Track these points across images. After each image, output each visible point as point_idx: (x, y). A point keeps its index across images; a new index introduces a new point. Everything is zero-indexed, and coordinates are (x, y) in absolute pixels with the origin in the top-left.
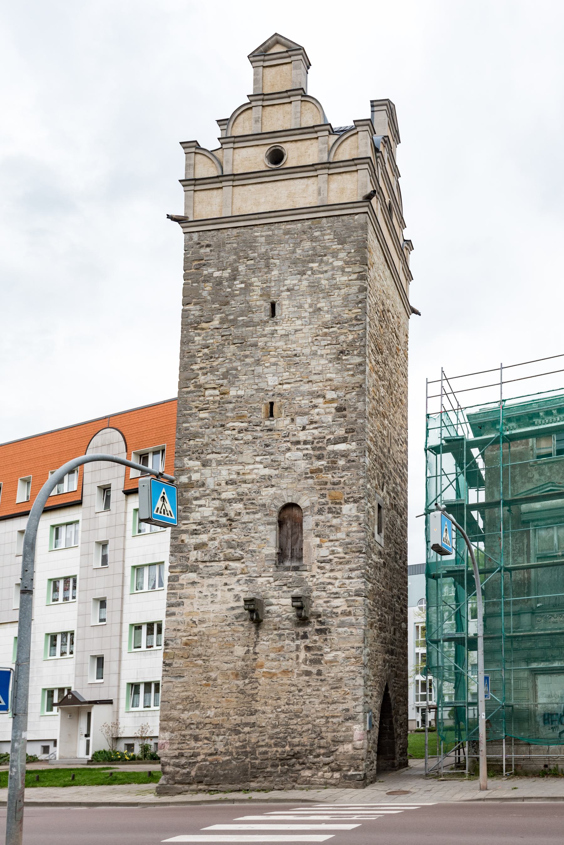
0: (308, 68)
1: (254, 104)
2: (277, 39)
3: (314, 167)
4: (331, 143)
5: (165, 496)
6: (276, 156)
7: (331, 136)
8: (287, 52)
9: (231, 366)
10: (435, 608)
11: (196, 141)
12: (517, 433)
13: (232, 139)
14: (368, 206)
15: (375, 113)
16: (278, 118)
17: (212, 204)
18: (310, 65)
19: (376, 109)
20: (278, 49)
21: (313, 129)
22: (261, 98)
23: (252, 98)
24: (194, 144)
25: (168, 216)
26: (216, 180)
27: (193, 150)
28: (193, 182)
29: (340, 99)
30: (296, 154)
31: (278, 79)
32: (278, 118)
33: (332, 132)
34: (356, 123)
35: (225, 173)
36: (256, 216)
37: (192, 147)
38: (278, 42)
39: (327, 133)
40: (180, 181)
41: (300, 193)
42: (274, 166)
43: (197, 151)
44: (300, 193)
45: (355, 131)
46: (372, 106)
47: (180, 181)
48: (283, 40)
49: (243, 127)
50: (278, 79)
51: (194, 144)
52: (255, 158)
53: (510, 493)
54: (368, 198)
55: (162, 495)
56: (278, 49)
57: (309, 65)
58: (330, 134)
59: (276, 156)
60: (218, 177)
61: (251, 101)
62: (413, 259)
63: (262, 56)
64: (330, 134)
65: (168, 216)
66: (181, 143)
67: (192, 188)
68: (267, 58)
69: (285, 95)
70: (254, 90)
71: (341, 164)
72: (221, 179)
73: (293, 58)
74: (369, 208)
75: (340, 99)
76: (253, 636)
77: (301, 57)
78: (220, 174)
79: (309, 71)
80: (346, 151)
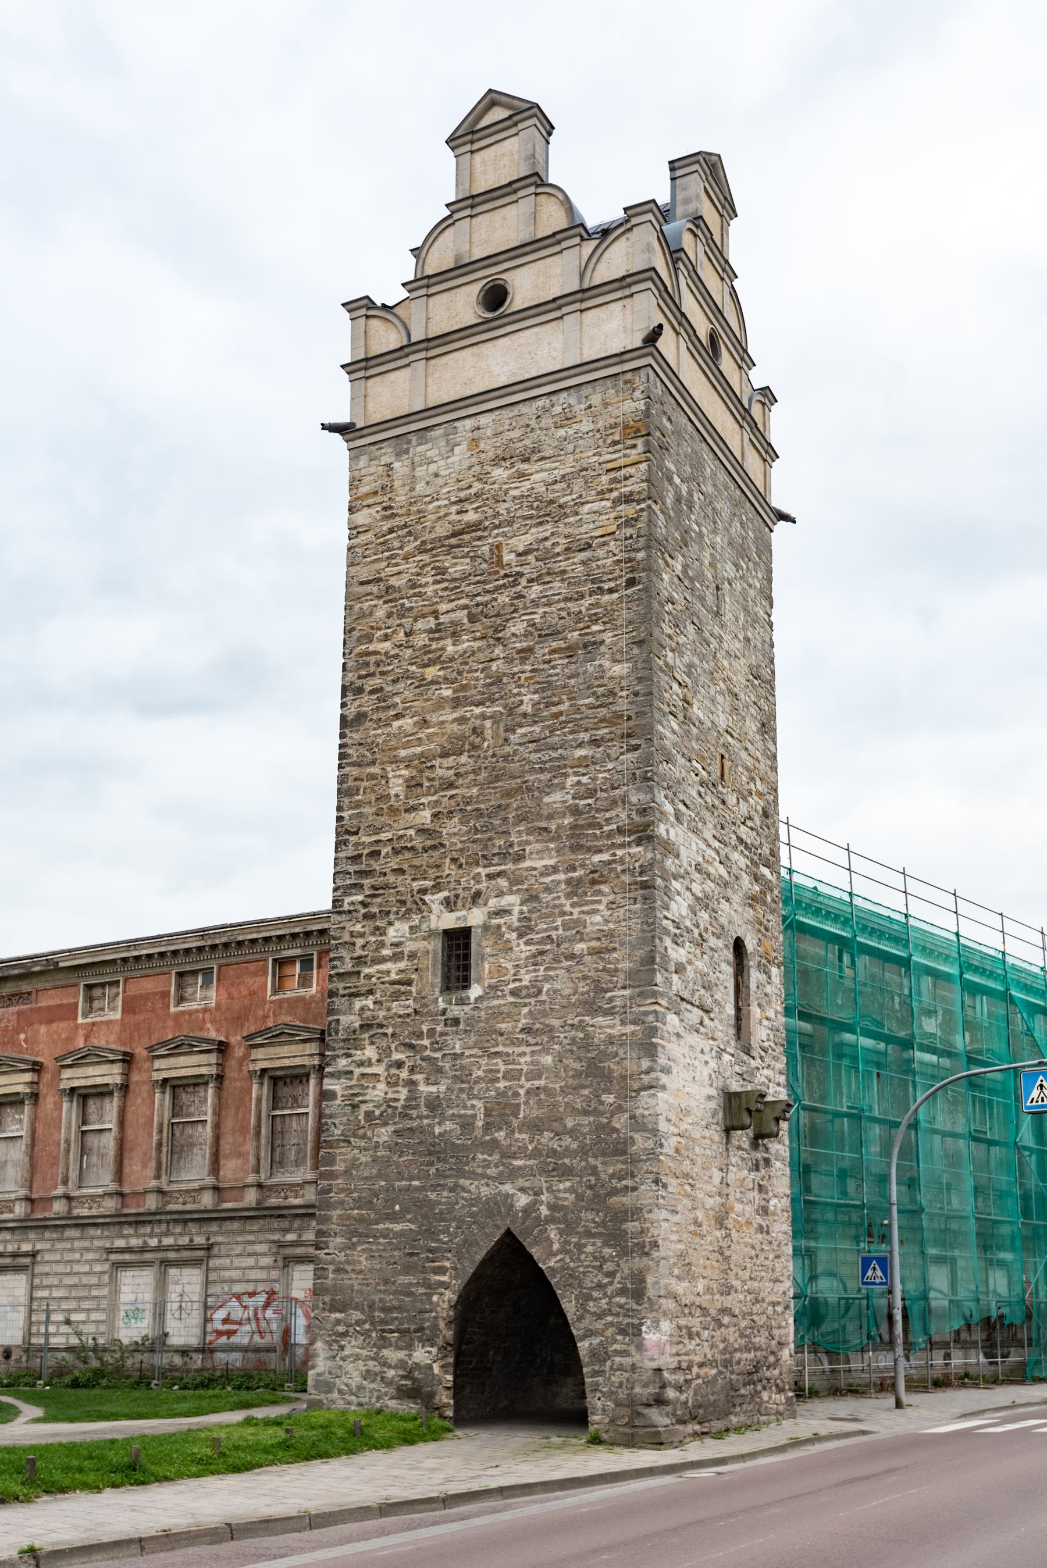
0: (550, 134)
1: (456, 216)
2: (492, 99)
3: (556, 303)
4: (585, 258)
6: (495, 297)
8: (510, 117)
11: (367, 297)
13: (425, 281)
14: (651, 354)
15: (678, 181)
16: (501, 228)
18: (553, 128)
19: (678, 173)
20: (498, 114)
21: (555, 238)
22: (469, 204)
23: (453, 208)
24: (365, 301)
25: (324, 427)
27: (363, 311)
29: (604, 173)
30: (526, 286)
31: (500, 163)
32: (501, 228)
33: (586, 236)
34: (629, 212)
35: (413, 340)
36: (463, 404)
37: (362, 308)
38: (493, 104)
39: (577, 240)
41: (540, 349)
42: (490, 315)
43: (371, 313)
44: (540, 349)
45: (629, 226)
46: (672, 169)
48: (504, 99)
49: (439, 259)
50: (500, 163)
51: (365, 301)
52: (461, 306)
54: (654, 336)
56: (498, 114)
57: (550, 128)
58: (583, 239)
59: (495, 297)
60: (402, 348)
61: (453, 212)
62: (779, 426)
63: (466, 138)
64: (583, 239)
65: (324, 427)
66: (404, 285)
67: (361, 374)
68: (476, 136)
69: (508, 189)
70: (457, 193)
71: (388, 357)
72: (407, 350)
73: (521, 126)
75: (604, 173)
76: (722, 1149)
77: (534, 121)
78: (405, 343)
79: (551, 139)
80: (617, 261)
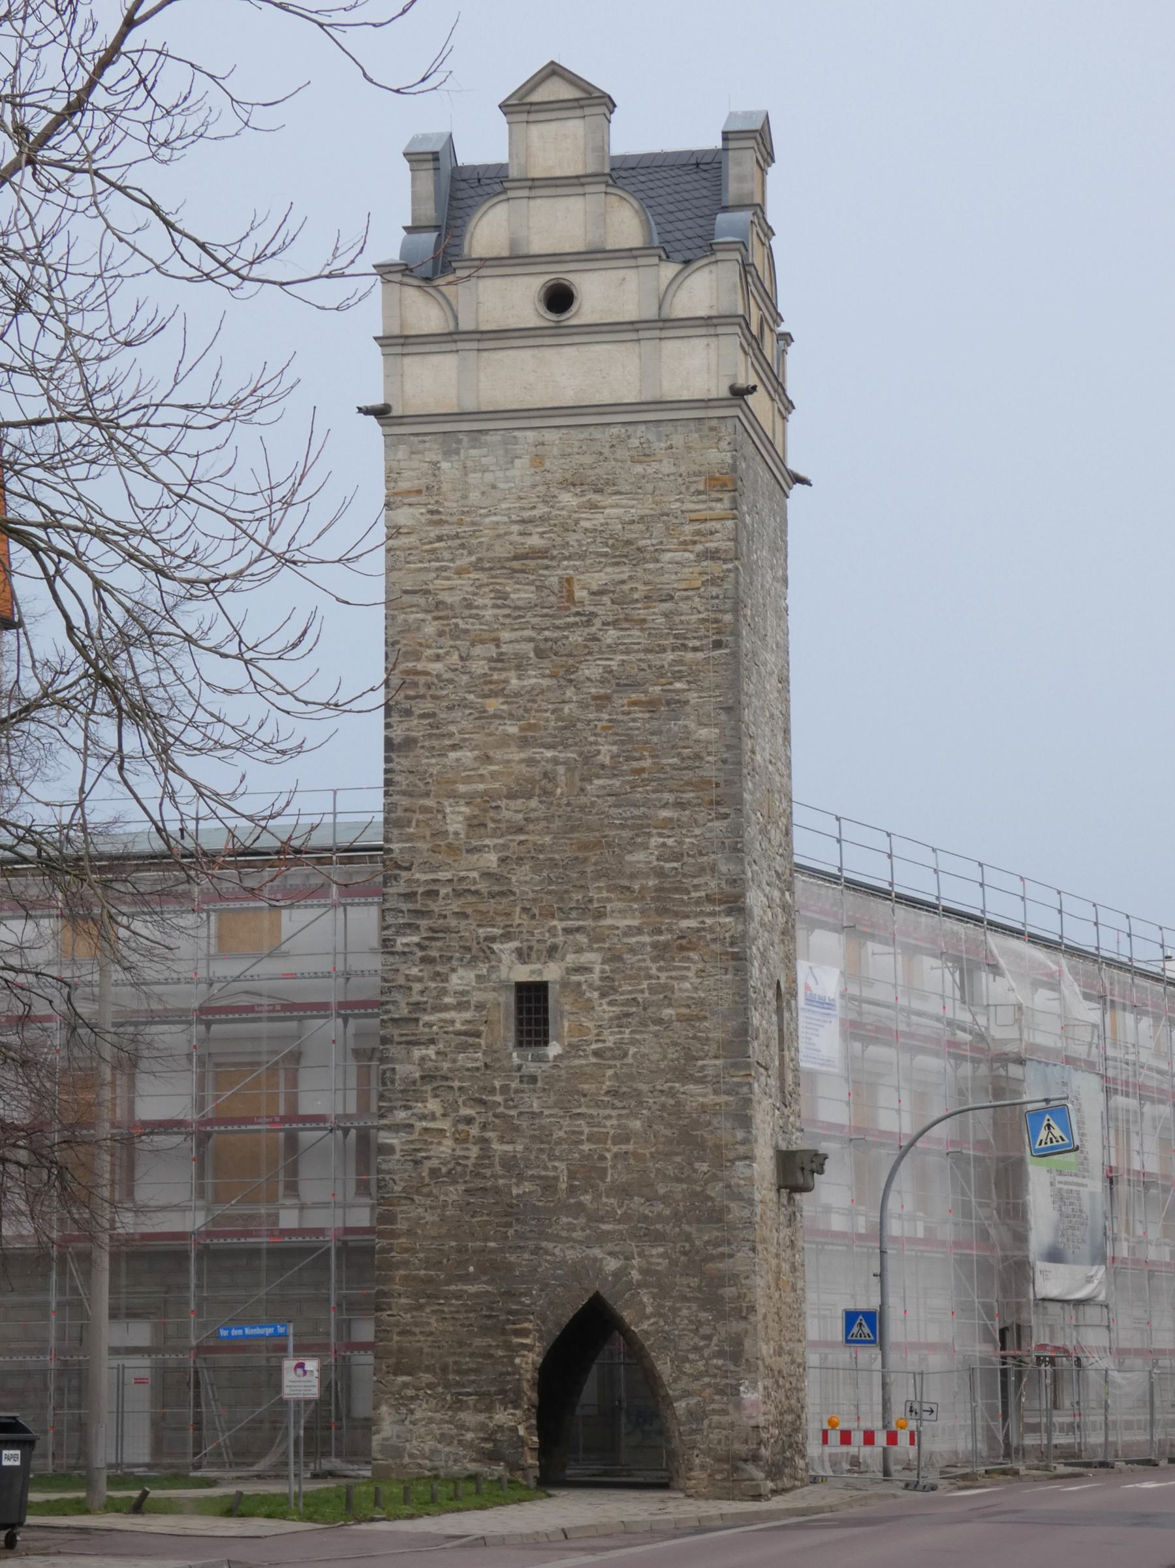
5: (1051, 1122)
6: (559, 299)
7: (663, 264)
9: (1093, 1404)
10: (894, 1228)
12: (160, 1499)
17: (434, 382)
18: (615, 106)
20: (557, 90)
25: (360, 410)
26: (449, 338)
28: (401, 341)
40: (376, 338)
47: (376, 338)
53: (928, 1046)
55: (1046, 1122)
56: (557, 90)
59: (559, 299)
65: (360, 410)
72: (456, 337)
74: (742, 410)
78: (452, 328)
